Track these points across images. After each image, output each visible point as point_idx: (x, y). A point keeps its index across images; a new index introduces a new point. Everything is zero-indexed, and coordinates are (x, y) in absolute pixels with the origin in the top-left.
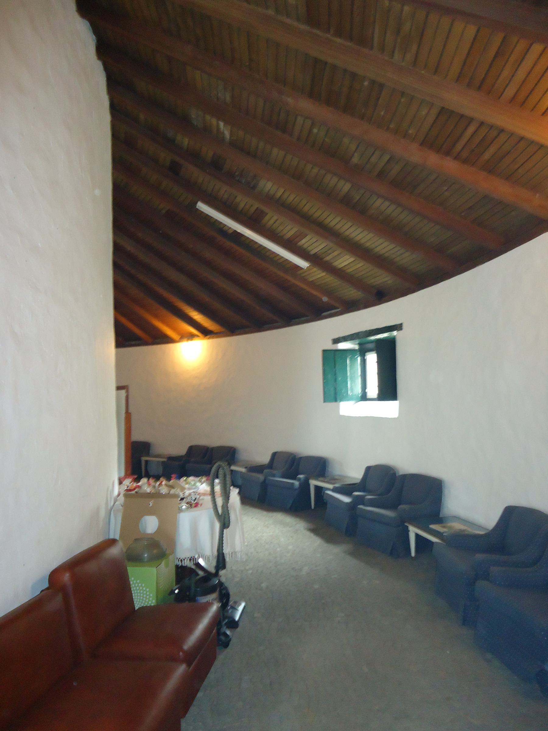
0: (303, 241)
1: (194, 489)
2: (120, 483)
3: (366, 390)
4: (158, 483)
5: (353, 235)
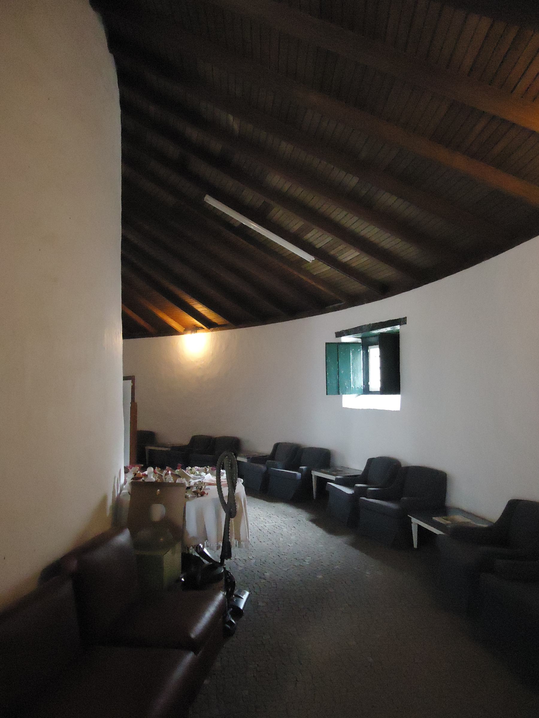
0: (309, 235)
1: (199, 478)
2: (126, 472)
3: (369, 383)
4: (165, 472)
5: (358, 230)
